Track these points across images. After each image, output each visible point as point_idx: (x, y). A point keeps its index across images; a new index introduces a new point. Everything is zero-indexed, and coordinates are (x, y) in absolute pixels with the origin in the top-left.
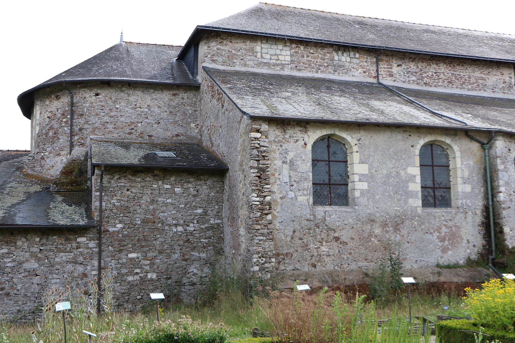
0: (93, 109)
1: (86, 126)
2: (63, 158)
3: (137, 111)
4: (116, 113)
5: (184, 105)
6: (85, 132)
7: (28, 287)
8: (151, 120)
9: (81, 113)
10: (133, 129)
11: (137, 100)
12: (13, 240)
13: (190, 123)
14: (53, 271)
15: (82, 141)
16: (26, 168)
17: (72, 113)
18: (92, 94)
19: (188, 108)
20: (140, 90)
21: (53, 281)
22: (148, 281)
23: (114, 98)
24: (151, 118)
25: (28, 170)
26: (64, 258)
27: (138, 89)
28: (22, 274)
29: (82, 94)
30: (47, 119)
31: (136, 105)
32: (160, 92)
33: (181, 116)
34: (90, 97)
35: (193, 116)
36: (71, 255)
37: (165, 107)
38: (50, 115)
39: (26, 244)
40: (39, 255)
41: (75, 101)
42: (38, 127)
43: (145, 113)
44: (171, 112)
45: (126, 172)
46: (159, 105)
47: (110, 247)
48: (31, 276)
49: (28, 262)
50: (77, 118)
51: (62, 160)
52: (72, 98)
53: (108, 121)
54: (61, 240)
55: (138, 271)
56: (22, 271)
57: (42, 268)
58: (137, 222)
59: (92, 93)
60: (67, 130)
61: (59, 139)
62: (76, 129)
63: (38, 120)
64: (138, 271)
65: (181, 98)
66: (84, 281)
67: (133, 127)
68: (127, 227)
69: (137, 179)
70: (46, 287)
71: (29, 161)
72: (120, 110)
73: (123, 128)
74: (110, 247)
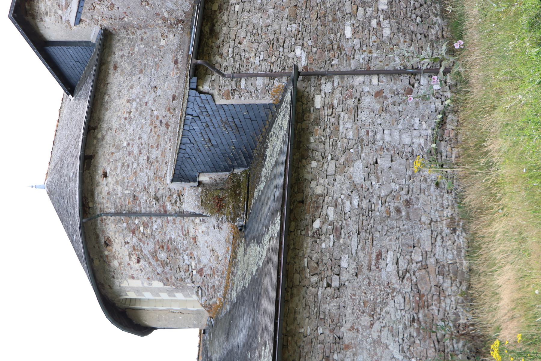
0: (126, 180)
1: (152, 191)
2: (200, 231)
3: (135, 116)
4: (136, 146)
5: (132, 54)
6: (161, 192)
7: (396, 175)
8: (149, 98)
9: (131, 200)
10: (161, 122)
11: (118, 117)
12: (314, 200)
13: (160, 47)
14: (371, 139)
15: (175, 196)
16: (214, 300)
17: (130, 214)
18: (103, 182)
19: (136, 49)
20: (104, 114)
21: (387, 138)
22: (392, 8)
23: (113, 150)
24: (147, 97)
25: (218, 297)
26: (348, 125)
27: (102, 117)
28: (374, 183)
29: (103, 198)
30: (141, 263)
31: (126, 119)
32: (109, 86)
33: (148, 58)
34: (109, 185)
35: (149, 42)
36: (344, 116)
37: (132, 79)
38: (134, 258)
39: (322, 181)
40: (342, 160)
41: (113, 211)
42: (153, 282)
43: (139, 105)
44: (141, 72)
45: (212, 47)
46: (129, 87)
47: (333, 63)
48: (377, 170)
49: (353, 177)
50: (139, 205)
51: (202, 232)
52: (107, 214)
53: (145, 158)
54: (317, 130)
55: (374, 23)
56: (368, 184)
57: (363, 155)
58: (294, 29)
59: (101, 182)
60: (157, 223)
61: (171, 238)
62: (156, 207)
63: (143, 283)
64: (374, 23)
65: (121, 58)
66: (389, 95)
67: (158, 122)
68: (301, 42)
69: (224, 32)
70: (398, 149)
71: (204, 295)
72: (131, 140)
73: (158, 136)
74: (333, 63)
